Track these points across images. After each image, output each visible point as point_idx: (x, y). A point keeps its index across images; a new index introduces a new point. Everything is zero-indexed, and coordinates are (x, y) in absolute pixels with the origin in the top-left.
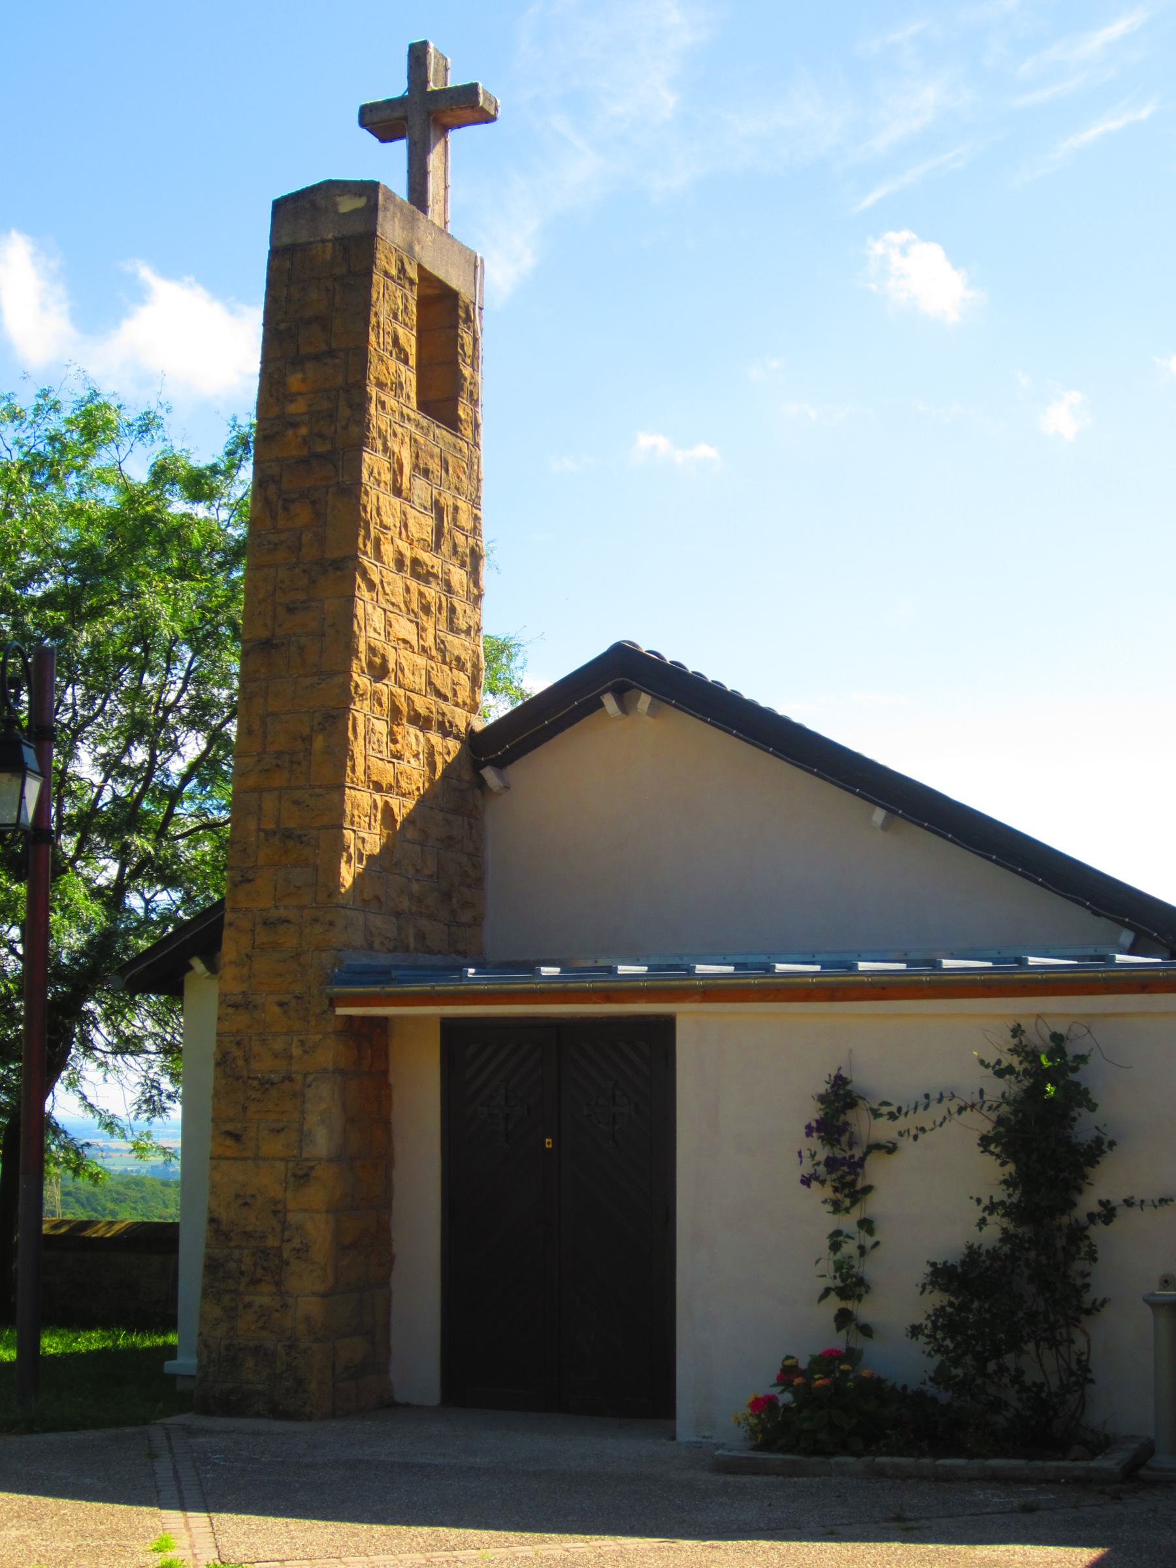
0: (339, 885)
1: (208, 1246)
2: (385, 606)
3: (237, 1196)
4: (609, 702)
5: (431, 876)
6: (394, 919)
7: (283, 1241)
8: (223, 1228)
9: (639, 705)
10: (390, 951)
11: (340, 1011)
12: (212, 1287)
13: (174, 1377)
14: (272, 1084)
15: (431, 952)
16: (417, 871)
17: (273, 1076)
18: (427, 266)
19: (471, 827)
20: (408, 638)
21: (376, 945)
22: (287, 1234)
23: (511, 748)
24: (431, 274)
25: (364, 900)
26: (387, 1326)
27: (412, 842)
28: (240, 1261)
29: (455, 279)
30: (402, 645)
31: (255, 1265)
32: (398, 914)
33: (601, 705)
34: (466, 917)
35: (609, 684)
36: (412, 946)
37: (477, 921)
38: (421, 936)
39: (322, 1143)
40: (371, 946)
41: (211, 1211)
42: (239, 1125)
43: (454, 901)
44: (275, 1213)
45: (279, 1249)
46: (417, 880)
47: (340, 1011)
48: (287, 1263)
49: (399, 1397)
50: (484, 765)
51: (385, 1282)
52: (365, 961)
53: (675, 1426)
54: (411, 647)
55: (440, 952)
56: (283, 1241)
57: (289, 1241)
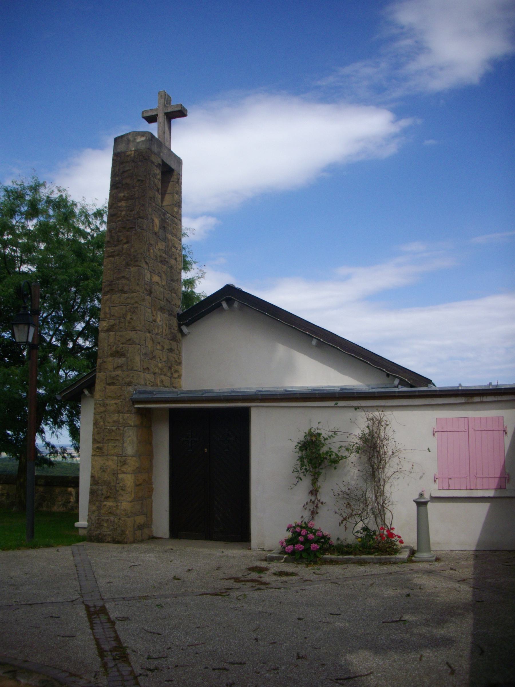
0: (8, 430)
1: (91, 485)
2: (151, 271)
3: (101, 468)
4: (225, 305)
5: (165, 361)
6: (153, 375)
7: (116, 483)
8: (96, 479)
9: (234, 305)
10: (152, 386)
11: (136, 406)
12: (92, 499)
13: (78, 528)
14: (113, 430)
15: (165, 387)
16: (161, 360)
17: (113, 428)
18: (165, 160)
19: (178, 345)
20: (158, 281)
21: (148, 384)
22: (118, 482)
23: (204, 311)
24: (166, 164)
25: (143, 369)
26: (151, 512)
27: (159, 350)
28: (102, 490)
29: (173, 166)
30: (156, 283)
31: (107, 492)
32: (155, 374)
33: (222, 305)
34: (176, 375)
35: (224, 298)
36: (159, 384)
37: (180, 377)
38: (162, 381)
39: (130, 450)
40: (146, 384)
41: (92, 474)
42: (102, 444)
43: (172, 370)
44: (114, 474)
45: (115, 486)
46: (161, 363)
47: (136, 406)
48: (118, 491)
49: (155, 535)
50: (182, 325)
51: (150, 497)
52: (144, 389)
53: (251, 545)
54: (159, 284)
55: (168, 387)
56: (116, 483)
57: (118, 483)
